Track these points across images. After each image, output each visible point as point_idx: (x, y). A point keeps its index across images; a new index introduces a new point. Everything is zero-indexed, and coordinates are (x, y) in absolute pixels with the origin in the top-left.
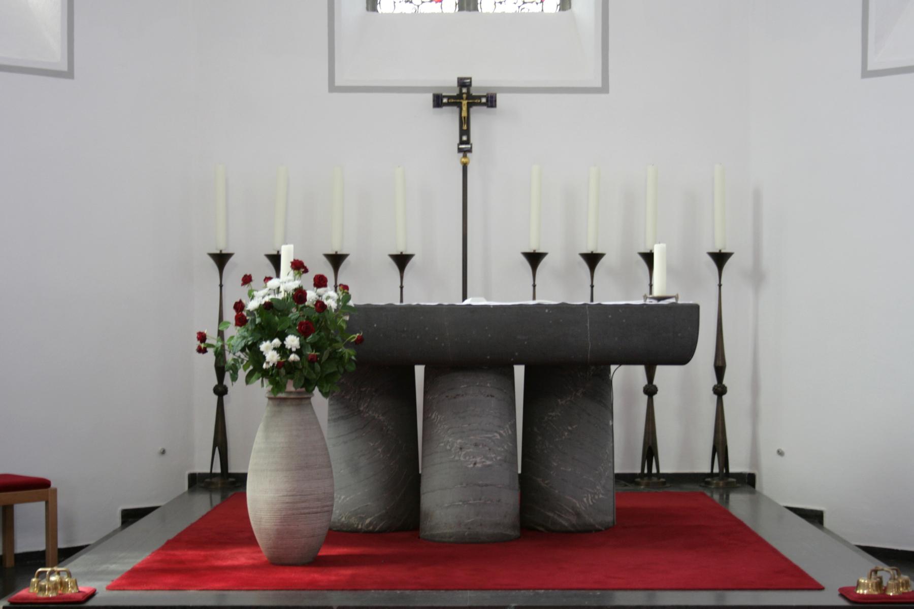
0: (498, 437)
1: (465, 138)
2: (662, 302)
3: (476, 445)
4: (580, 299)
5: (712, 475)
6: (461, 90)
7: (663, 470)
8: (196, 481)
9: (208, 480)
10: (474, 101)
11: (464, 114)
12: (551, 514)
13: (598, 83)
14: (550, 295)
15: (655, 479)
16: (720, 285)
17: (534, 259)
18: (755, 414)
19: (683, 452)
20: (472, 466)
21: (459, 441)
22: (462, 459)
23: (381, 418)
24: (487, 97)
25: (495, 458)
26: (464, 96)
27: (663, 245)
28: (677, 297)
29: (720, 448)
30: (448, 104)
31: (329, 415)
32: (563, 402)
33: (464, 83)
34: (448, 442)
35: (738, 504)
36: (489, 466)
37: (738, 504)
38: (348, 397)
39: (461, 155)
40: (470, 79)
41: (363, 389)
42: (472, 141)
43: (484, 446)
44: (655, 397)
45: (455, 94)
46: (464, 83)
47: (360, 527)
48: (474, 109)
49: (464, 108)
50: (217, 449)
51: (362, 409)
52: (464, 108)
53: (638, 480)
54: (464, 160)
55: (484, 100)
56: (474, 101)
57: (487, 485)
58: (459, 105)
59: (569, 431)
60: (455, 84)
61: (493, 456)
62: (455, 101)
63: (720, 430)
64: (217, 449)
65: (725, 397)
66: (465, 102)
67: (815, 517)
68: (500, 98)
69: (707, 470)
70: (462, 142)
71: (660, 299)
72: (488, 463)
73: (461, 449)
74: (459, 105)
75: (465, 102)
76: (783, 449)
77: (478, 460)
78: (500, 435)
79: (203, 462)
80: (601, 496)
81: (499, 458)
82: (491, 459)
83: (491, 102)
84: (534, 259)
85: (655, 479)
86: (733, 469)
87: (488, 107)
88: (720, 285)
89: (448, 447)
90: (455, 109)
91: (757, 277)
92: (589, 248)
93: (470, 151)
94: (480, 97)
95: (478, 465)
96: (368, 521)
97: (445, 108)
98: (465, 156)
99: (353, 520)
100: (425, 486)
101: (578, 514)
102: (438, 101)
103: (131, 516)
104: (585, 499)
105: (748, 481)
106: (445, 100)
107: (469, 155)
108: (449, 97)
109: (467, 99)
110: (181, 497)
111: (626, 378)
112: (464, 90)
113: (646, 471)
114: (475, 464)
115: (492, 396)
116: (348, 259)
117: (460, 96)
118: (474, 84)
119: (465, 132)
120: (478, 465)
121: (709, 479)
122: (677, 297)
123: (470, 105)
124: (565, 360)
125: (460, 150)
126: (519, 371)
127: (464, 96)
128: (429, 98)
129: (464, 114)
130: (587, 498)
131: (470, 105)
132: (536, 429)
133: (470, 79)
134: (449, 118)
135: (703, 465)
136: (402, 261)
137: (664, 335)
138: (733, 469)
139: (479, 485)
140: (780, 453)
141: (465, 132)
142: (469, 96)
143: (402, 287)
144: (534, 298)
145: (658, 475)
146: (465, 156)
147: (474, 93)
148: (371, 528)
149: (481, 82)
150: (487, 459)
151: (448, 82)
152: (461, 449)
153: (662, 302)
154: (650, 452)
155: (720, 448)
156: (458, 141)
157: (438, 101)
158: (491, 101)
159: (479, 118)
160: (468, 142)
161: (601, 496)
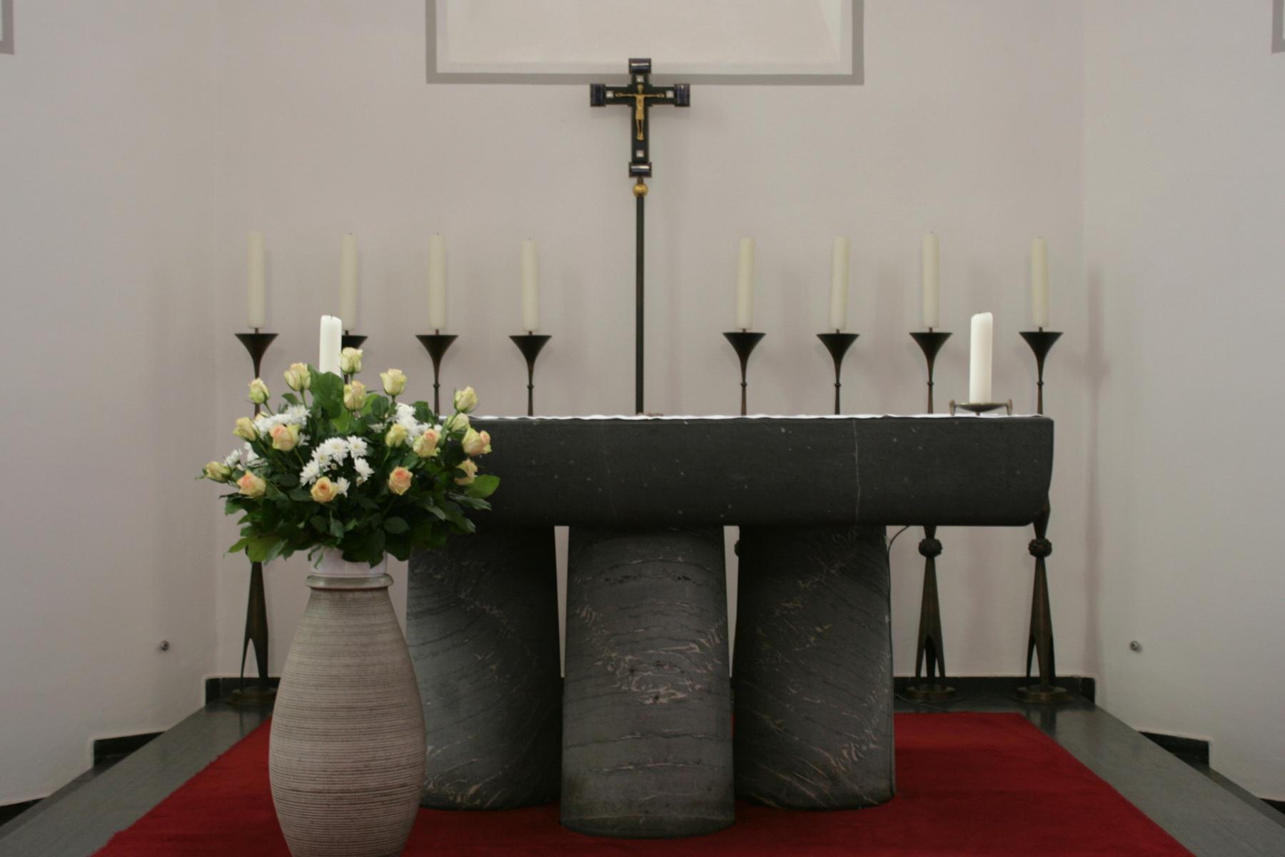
0: (698, 650)
1: (640, 154)
2: (983, 415)
3: (659, 665)
4: (816, 409)
5: (1027, 681)
6: (634, 79)
7: (949, 673)
8: (218, 691)
9: (237, 691)
10: (655, 96)
11: (640, 116)
12: (787, 778)
13: (847, 70)
14: (770, 404)
15: (938, 687)
16: (1040, 384)
17: (744, 343)
18: (1092, 582)
19: (985, 646)
20: (651, 701)
21: (629, 658)
22: (634, 689)
23: (495, 612)
24: (674, 89)
25: (692, 687)
26: (640, 87)
27: (988, 316)
28: (1009, 407)
29: (1040, 636)
30: (615, 101)
31: (409, 607)
32: (807, 585)
33: (641, 69)
34: (610, 659)
35: (1070, 730)
36: (681, 701)
37: (1070, 730)
38: (439, 577)
39: (635, 180)
40: (649, 61)
41: (464, 563)
42: (652, 159)
43: (672, 666)
44: (938, 559)
45: (625, 85)
46: (641, 69)
47: (459, 800)
48: (654, 109)
49: (640, 107)
50: (251, 642)
51: (462, 596)
52: (640, 107)
53: (912, 689)
54: (639, 188)
55: (670, 94)
56: (655, 96)
57: (677, 736)
58: (631, 102)
59: (818, 634)
60: (626, 70)
61: (688, 683)
62: (624, 96)
63: (1041, 609)
64: (251, 642)
65: (1048, 560)
66: (640, 98)
67: (1193, 752)
68: (695, 91)
69: (1020, 673)
70: (636, 161)
71: (978, 408)
72: (680, 695)
73: (632, 671)
74: (631, 102)
75: (640, 98)
76: (1140, 640)
77: (662, 690)
78: (701, 646)
79: (231, 661)
80: (872, 746)
81: (698, 687)
82: (683, 689)
83: (682, 97)
84: (744, 343)
85: (938, 687)
86: (1060, 671)
87: (677, 105)
88: (1040, 384)
89: (610, 669)
90: (626, 109)
91: (1095, 369)
92: (833, 325)
93: (648, 174)
94: (664, 90)
95: (663, 700)
96: (472, 790)
97: (609, 107)
98: (640, 183)
99: (448, 789)
100: (572, 732)
101: (834, 779)
102: (599, 96)
103: (110, 752)
104: (845, 753)
105: (1083, 690)
106: (610, 95)
107: (646, 180)
108: (615, 90)
109: (644, 92)
110: (196, 716)
111: (904, 541)
112: (640, 79)
113: (924, 674)
114: (657, 698)
115: (687, 579)
116: (456, 342)
117: (633, 88)
118: (654, 70)
119: (640, 143)
120: (663, 700)
121: (1023, 689)
122: (1009, 407)
123: (648, 103)
124: (808, 511)
125: (633, 174)
126: (732, 534)
127: (640, 87)
128: (585, 91)
129: (640, 116)
130: (851, 743)
131: (648, 103)
132: (759, 631)
133: (649, 61)
134: (616, 122)
135: (1010, 662)
136: (531, 345)
137: (999, 473)
138: (1060, 671)
139: (665, 736)
140: (1135, 647)
141: (640, 143)
142: (648, 88)
143: (530, 387)
144: (837, 412)
145: (944, 681)
146: (640, 183)
147: (654, 83)
148: (478, 802)
149: (668, 62)
150: (679, 689)
151: (612, 63)
152: (632, 671)
153: (983, 415)
154: (930, 644)
155: (1040, 636)
156: (629, 159)
157: (599, 96)
158: (681, 98)
159: (662, 122)
160: (645, 161)
161: (872, 746)
